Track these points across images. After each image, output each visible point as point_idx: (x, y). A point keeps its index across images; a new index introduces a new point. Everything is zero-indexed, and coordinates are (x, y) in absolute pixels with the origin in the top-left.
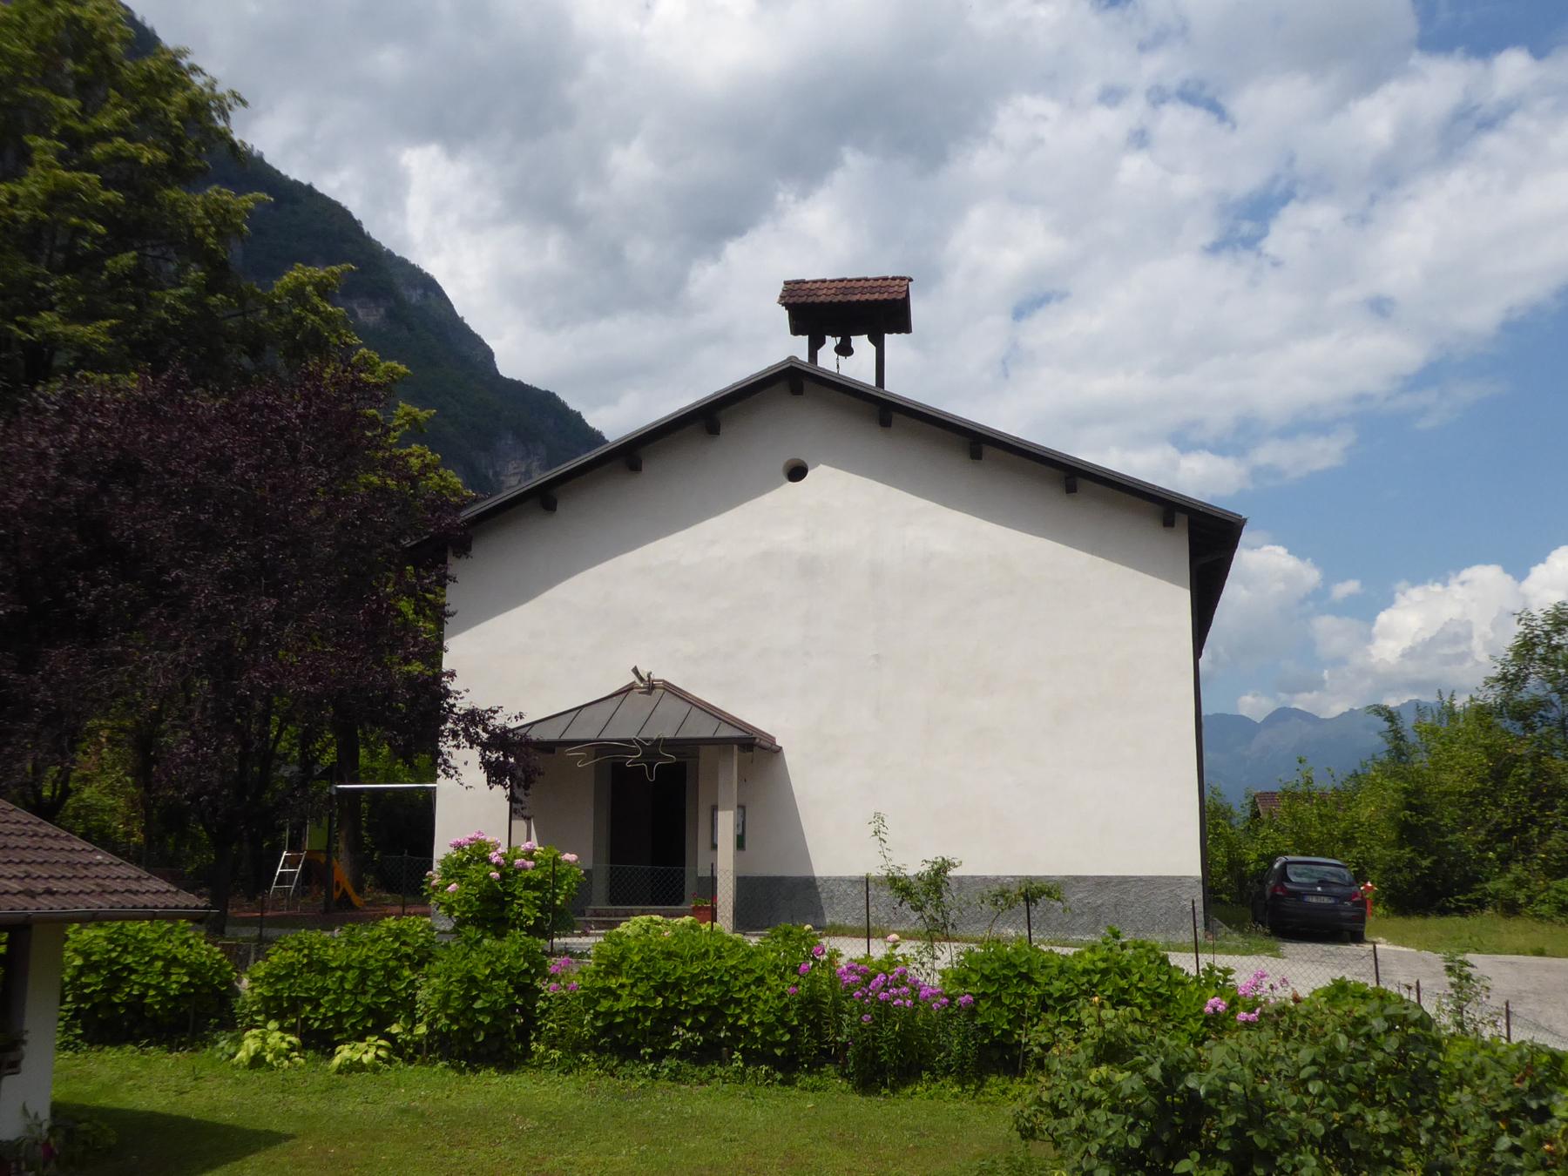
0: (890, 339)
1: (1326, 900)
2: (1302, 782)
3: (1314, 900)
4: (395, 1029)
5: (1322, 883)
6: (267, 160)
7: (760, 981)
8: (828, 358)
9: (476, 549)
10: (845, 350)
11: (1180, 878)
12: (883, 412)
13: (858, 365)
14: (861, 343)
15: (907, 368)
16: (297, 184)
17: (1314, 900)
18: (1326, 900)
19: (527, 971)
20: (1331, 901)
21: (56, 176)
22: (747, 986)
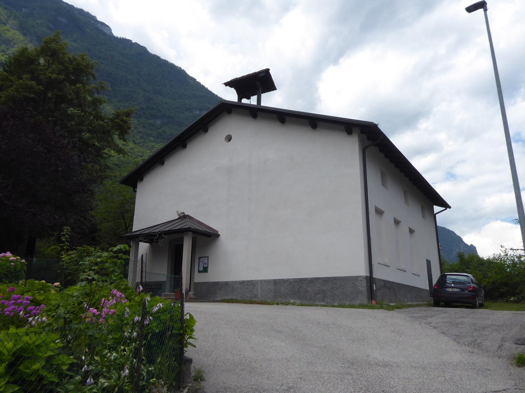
1: (456, 290)
3: (450, 290)
5: (453, 283)
9: (145, 179)
11: (357, 277)
12: (258, 113)
17: (450, 290)
18: (456, 290)
20: (459, 290)
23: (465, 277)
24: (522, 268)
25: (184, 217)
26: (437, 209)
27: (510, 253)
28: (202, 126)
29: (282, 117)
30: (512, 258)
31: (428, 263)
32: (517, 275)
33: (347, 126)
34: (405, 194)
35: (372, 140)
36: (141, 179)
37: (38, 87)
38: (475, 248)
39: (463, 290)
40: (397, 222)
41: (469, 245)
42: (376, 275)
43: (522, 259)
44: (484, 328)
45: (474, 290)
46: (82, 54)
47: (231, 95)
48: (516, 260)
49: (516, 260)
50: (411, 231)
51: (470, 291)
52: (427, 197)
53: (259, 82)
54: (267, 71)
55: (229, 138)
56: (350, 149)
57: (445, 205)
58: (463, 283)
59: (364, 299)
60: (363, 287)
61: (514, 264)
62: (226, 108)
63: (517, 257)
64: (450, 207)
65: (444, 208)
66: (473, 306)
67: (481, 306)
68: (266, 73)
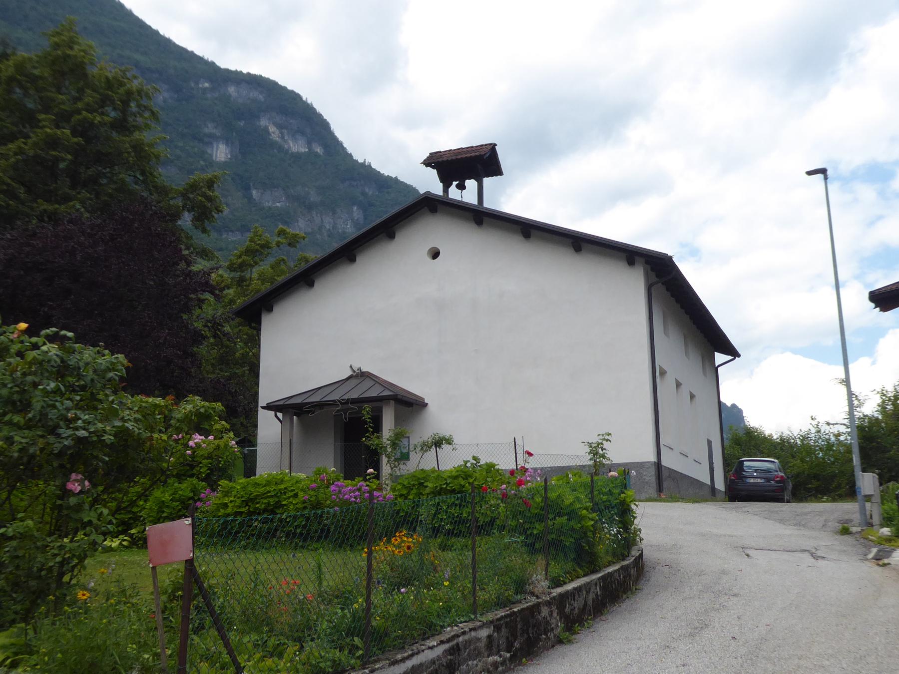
0: (487, 181)
1: (759, 480)
2: (813, 430)
3: (752, 481)
4: (133, 531)
5: (756, 471)
6: (373, 166)
7: (296, 496)
8: (454, 193)
9: (276, 309)
10: (461, 187)
11: (642, 463)
12: (481, 217)
13: (468, 194)
14: (471, 184)
15: (510, 196)
16: (389, 177)
17: (752, 481)
18: (759, 480)
19: (192, 498)
20: (762, 481)
21: (46, 132)
22: (289, 498)
23: (769, 464)
24: (840, 453)
25: (360, 376)
26: (720, 358)
27: (824, 428)
28: (386, 229)
29: (527, 229)
30: (827, 437)
31: (710, 443)
32: (833, 463)
33: (630, 255)
34: (685, 338)
35: (663, 279)
36: (270, 310)
37: (75, 140)
38: (740, 411)
39: (768, 480)
40: (678, 385)
41: (729, 405)
42: (665, 462)
43: (842, 438)
44: (806, 514)
45: (782, 480)
46: (123, 68)
47: (429, 182)
48: (833, 439)
49: (833, 439)
50: (692, 397)
51: (777, 482)
52: (706, 337)
53: (479, 163)
54: (493, 147)
55: (435, 254)
56: (632, 286)
57: (732, 352)
58: (768, 471)
59: (652, 491)
60: (650, 476)
61: (830, 446)
62: (429, 205)
63: (835, 435)
64: (739, 356)
65: (731, 358)
66: (781, 500)
67: (788, 502)
68: (492, 149)
